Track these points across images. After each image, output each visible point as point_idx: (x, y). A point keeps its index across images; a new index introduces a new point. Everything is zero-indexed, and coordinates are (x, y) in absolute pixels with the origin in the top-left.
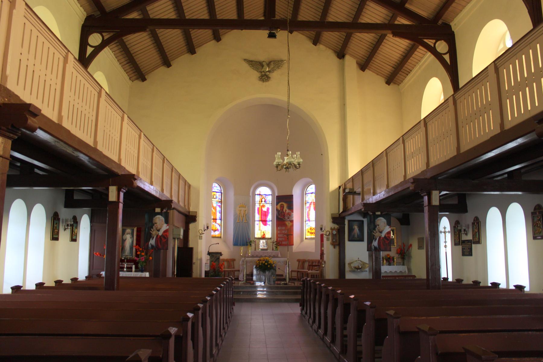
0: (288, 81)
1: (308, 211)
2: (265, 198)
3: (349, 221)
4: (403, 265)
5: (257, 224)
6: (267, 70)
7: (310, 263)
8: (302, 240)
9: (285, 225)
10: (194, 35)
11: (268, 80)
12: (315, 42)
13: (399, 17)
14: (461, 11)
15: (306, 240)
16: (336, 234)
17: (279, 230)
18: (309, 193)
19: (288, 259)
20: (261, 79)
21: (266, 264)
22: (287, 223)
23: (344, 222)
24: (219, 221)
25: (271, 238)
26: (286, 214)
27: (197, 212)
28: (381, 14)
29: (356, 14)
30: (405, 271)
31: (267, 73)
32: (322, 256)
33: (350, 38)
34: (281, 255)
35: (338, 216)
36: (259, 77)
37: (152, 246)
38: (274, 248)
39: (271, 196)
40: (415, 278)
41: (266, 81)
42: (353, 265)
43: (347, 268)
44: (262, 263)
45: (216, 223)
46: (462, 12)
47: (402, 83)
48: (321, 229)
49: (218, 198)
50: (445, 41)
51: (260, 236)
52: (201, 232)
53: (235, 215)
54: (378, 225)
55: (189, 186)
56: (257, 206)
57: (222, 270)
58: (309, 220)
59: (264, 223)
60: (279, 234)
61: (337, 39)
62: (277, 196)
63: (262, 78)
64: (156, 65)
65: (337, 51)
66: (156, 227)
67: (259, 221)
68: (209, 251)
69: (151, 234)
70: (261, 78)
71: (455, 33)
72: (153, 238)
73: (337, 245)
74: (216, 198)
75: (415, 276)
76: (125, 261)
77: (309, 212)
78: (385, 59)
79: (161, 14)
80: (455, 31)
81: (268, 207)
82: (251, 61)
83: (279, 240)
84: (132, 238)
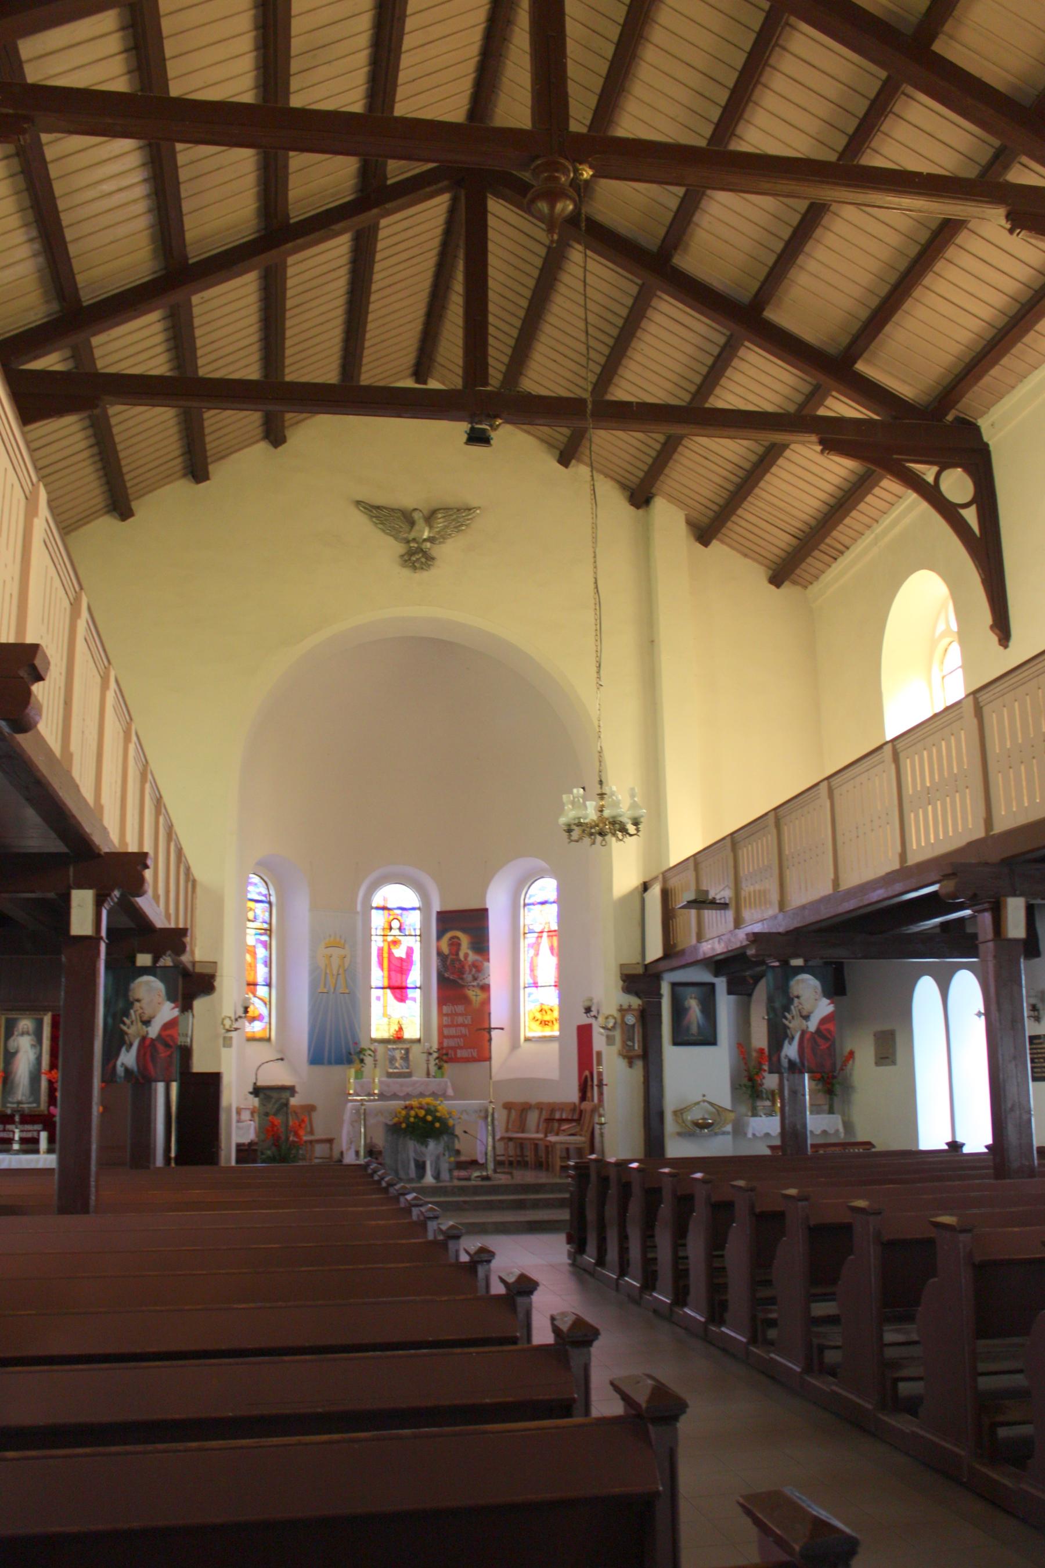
0: (593, 580)
1: (532, 958)
2: (399, 917)
3: (674, 985)
4: (831, 1111)
5: (378, 998)
6: (426, 535)
7: (544, 1112)
8: (515, 1044)
9: (465, 1000)
10: (212, 425)
11: (429, 566)
12: (565, 459)
13: (833, 397)
14: (1013, 387)
15: (529, 1045)
16: (633, 1026)
17: (447, 1015)
18: (533, 904)
19: (491, 1102)
20: (406, 561)
21: (429, 1118)
22: (471, 993)
23: (659, 988)
24: (262, 991)
25: (419, 1041)
26: (467, 968)
27: (216, 963)
28: (778, 386)
29: (607, 361)
30: (837, 1131)
31: (425, 544)
32: (653, 1090)
33: (675, 450)
34: (454, 1088)
35: (640, 970)
36: (402, 556)
37: (127, 1071)
38: (433, 1069)
39: (418, 912)
40: (873, 1150)
41: (422, 568)
42: (689, 1117)
43: (670, 1125)
44: (416, 1116)
45: (255, 996)
46: (1015, 391)
47: (815, 583)
48: (588, 1010)
49: (261, 920)
50: (967, 470)
51: (385, 1035)
52: (227, 1023)
53: (314, 970)
54: (798, 997)
55: (194, 881)
56: (377, 943)
57: (301, 1139)
58: (535, 985)
59: (399, 996)
60: (447, 1026)
61: (632, 451)
62: (438, 913)
63: (410, 559)
64: (88, 512)
65: (628, 483)
66: (140, 1011)
67: (383, 988)
68: (259, 1084)
69: (123, 1033)
70: (406, 558)
71: (991, 448)
72: (131, 1045)
73: (638, 1057)
74: (255, 920)
75: (869, 1144)
76: (17, 1118)
77: (535, 958)
78: (774, 512)
79: (650, 447)
80: (990, 443)
81: (409, 944)
82: (378, 508)
83: (445, 1045)
84: (38, 1048)
